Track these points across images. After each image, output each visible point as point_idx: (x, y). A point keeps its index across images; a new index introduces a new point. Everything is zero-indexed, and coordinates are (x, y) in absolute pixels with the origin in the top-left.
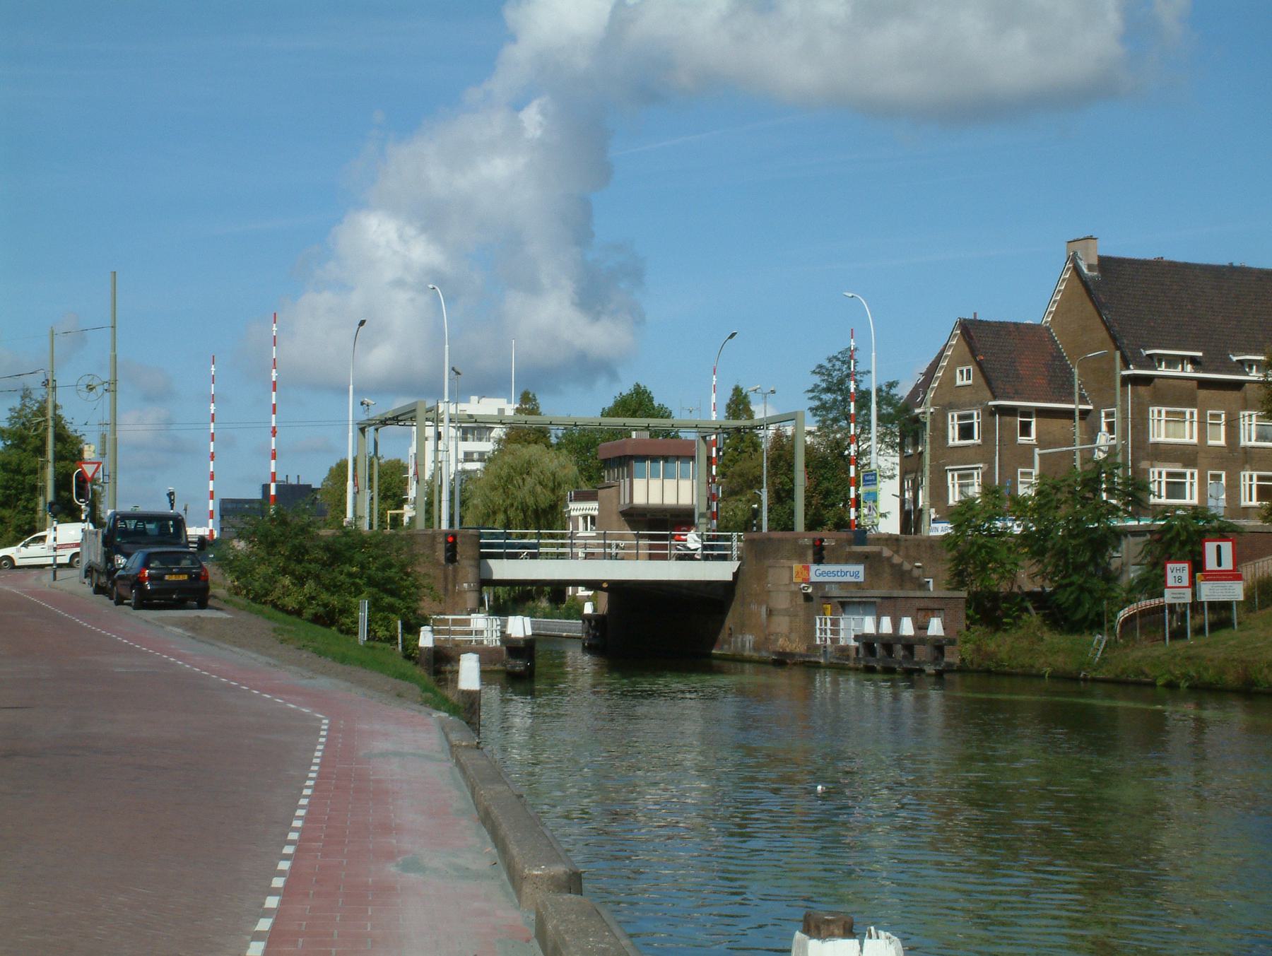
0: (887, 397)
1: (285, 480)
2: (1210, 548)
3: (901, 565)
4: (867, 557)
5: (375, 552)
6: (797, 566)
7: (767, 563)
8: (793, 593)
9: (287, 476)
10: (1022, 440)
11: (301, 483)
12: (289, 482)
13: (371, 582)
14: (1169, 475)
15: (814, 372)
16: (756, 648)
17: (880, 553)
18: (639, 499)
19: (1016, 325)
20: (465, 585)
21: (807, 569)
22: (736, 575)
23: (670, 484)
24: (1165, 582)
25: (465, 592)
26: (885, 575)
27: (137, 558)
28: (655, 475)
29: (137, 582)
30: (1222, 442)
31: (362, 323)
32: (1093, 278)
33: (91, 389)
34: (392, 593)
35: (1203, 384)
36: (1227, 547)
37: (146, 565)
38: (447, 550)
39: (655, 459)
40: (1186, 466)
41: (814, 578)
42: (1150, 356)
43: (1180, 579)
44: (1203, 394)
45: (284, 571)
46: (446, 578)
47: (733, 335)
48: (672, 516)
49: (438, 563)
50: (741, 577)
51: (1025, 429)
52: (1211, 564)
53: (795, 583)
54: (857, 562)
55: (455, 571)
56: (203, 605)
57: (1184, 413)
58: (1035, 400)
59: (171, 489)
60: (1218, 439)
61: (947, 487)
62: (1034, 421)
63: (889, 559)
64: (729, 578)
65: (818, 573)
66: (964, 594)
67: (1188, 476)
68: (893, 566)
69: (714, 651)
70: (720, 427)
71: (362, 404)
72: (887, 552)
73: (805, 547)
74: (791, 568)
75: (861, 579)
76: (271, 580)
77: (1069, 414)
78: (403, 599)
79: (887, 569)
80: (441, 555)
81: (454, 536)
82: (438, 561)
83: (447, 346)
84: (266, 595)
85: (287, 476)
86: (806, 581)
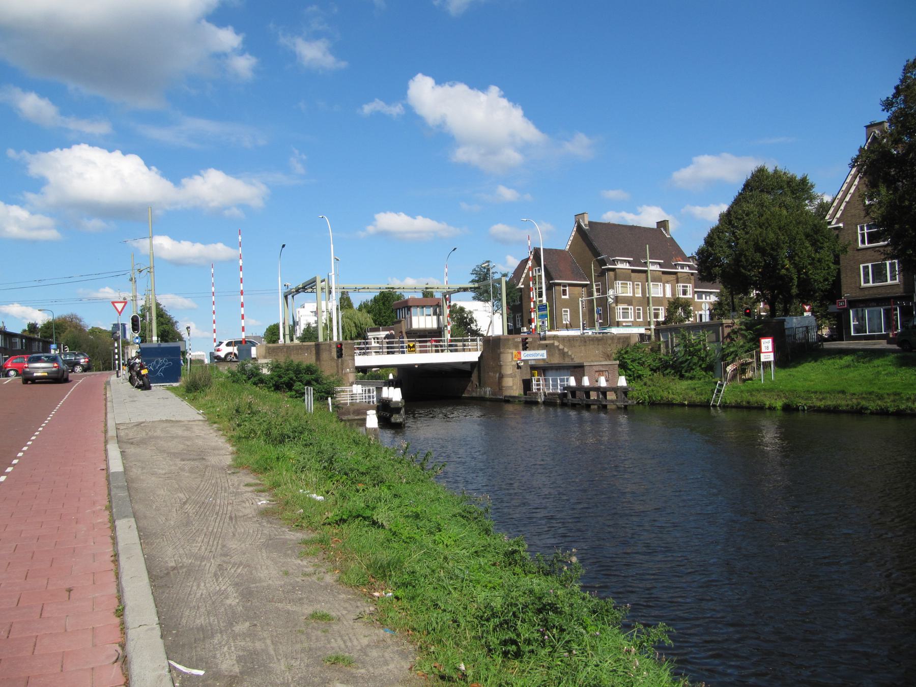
6: (515, 352)
10: (563, 297)
14: (623, 309)
15: (472, 274)
16: (494, 393)
17: (553, 344)
19: (556, 250)
20: (348, 370)
21: (520, 353)
24: (761, 349)
30: (640, 295)
33: (141, 272)
35: (633, 271)
38: (338, 352)
40: (629, 305)
41: (523, 358)
42: (613, 260)
43: (768, 347)
44: (633, 275)
46: (337, 366)
47: (455, 249)
48: (429, 333)
49: (332, 359)
51: (564, 292)
54: (543, 349)
57: (627, 284)
58: (568, 280)
59: (188, 325)
60: (639, 294)
62: (567, 288)
63: (558, 347)
64: (477, 360)
66: (618, 362)
68: (559, 350)
69: (463, 395)
71: (285, 285)
72: (556, 343)
73: (518, 342)
81: (341, 344)
83: (332, 246)
86: (520, 359)
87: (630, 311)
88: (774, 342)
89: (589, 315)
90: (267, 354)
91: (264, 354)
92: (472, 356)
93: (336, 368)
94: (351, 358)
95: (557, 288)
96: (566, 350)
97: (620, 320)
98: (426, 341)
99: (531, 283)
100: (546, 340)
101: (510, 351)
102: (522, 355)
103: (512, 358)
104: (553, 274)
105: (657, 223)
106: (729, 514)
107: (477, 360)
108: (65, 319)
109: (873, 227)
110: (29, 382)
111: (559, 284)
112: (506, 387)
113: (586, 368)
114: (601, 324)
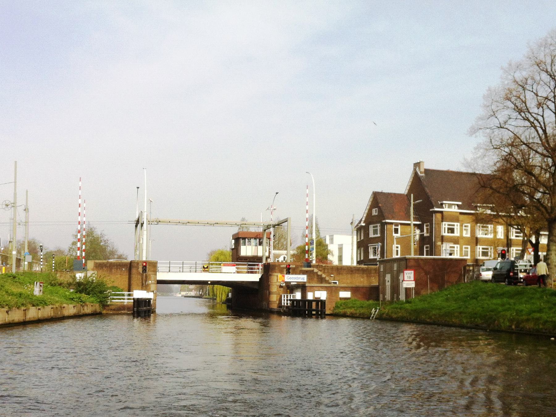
0: (533, 233)
3: (325, 278)
4: (307, 272)
6: (280, 275)
17: (313, 271)
19: (395, 194)
21: (284, 276)
25: (150, 284)
26: (315, 279)
31: (277, 193)
32: (422, 176)
38: (143, 268)
41: (286, 280)
43: (410, 277)
44: (462, 217)
46: (142, 279)
51: (396, 231)
53: (279, 282)
61: (369, 252)
62: (399, 227)
63: (317, 273)
67: (489, 249)
68: (318, 275)
70: (208, 223)
73: (283, 268)
74: (277, 276)
77: (409, 225)
79: (316, 276)
82: (139, 273)
87: (455, 249)
89: (419, 252)
90: (95, 268)
91: (92, 267)
92: (255, 278)
93: (141, 280)
94: (153, 273)
95: (389, 226)
96: (324, 276)
97: (478, 258)
98: (254, 265)
100: (311, 267)
101: (276, 274)
103: (277, 279)
104: (386, 214)
105: (414, 164)
106: (540, 405)
107: (258, 280)
108: (419, 247)
110: (209, 282)
111: (392, 223)
112: (273, 301)
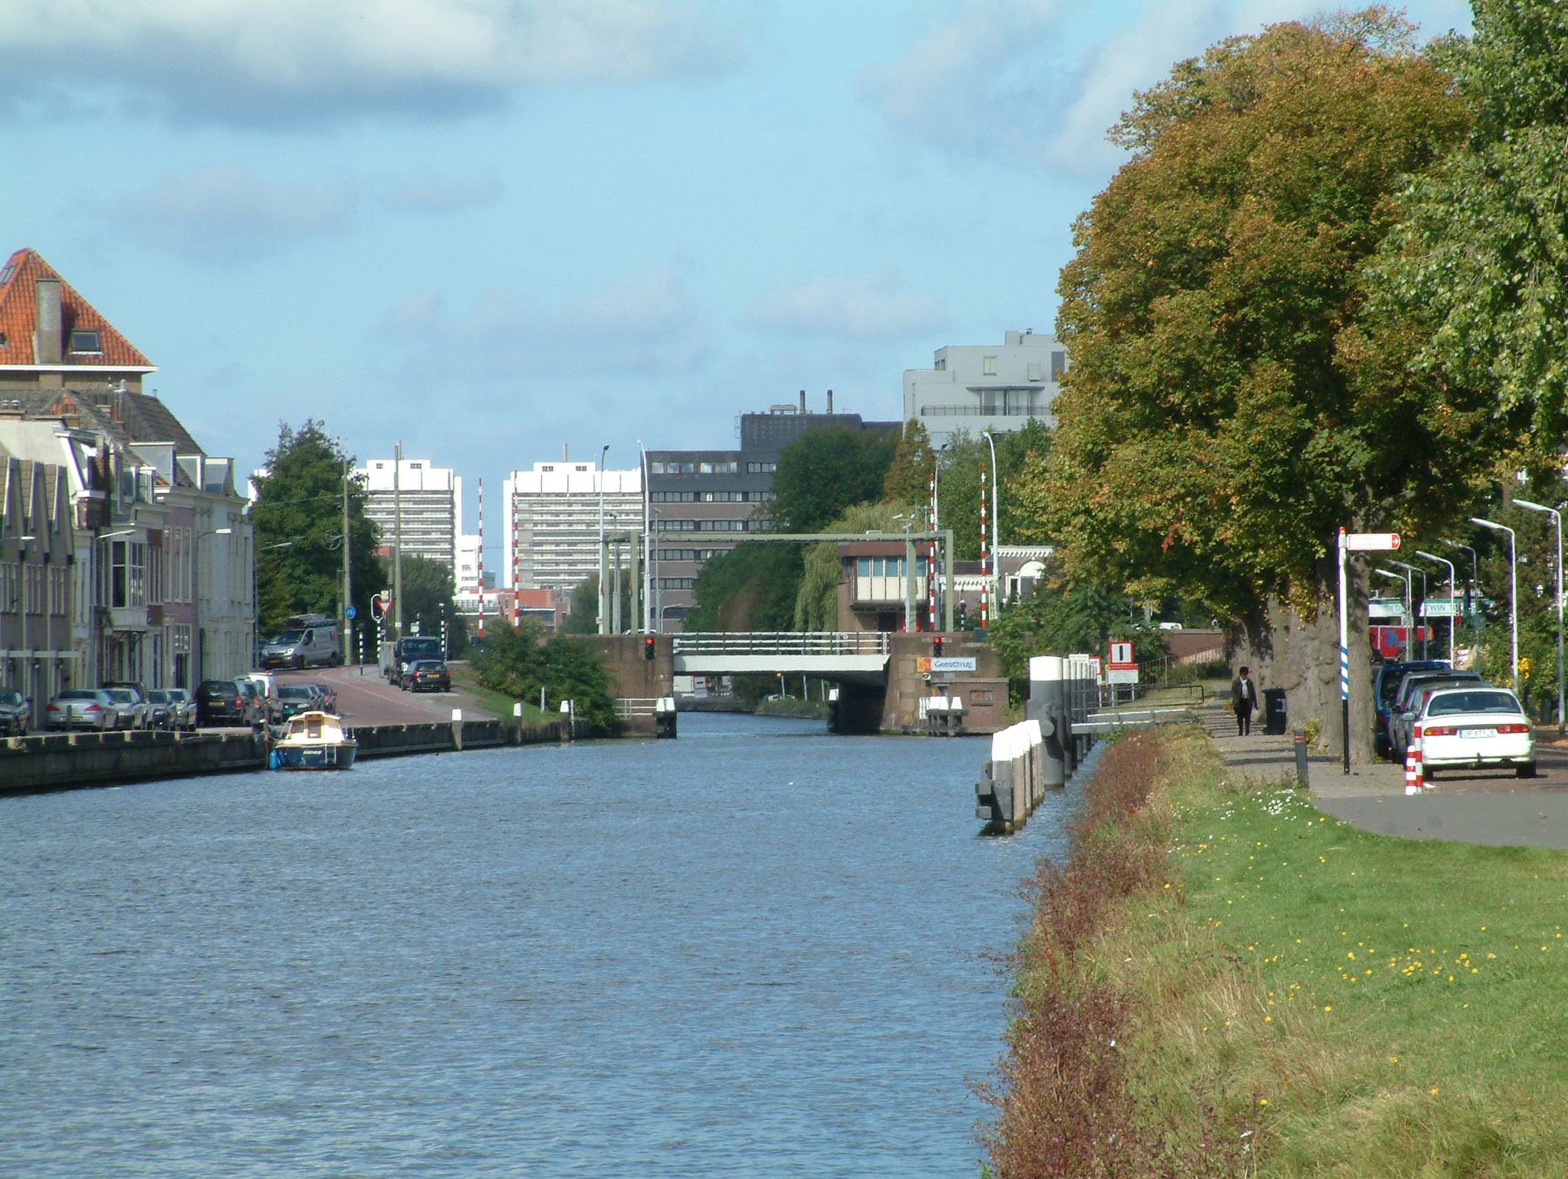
1: (798, 404)
2: (1115, 648)
5: (573, 654)
6: (920, 660)
7: (900, 656)
8: (919, 681)
9: (803, 393)
11: (837, 411)
12: (808, 408)
13: (571, 675)
18: (863, 595)
21: (929, 661)
22: (887, 666)
23: (893, 581)
27: (414, 664)
28: (877, 573)
29: (413, 678)
31: (606, 448)
34: (586, 683)
36: (1127, 647)
37: (417, 670)
39: (877, 558)
41: (934, 669)
45: (513, 669)
46: (646, 671)
49: (638, 659)
50: (891, 668)
52: (1116, 658)
54: (971, 656)
55: (653, 665)
56: (447, 690)
65: (937, 664)
66: (1006, 680)
75: (974, 669)
76: (503, 675)
78: (593, 687)
80: (642, 654)
84: (500, 684)
85: (803, 393)
88: (1041, 652)
99: (1383, 542)
102: (932, 665)
109: (214, 754)
113: (1287, 693)
114: (407, 652)
